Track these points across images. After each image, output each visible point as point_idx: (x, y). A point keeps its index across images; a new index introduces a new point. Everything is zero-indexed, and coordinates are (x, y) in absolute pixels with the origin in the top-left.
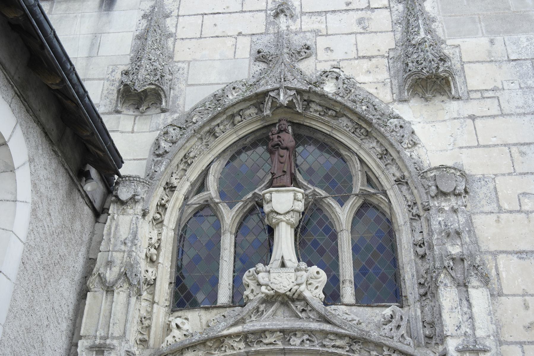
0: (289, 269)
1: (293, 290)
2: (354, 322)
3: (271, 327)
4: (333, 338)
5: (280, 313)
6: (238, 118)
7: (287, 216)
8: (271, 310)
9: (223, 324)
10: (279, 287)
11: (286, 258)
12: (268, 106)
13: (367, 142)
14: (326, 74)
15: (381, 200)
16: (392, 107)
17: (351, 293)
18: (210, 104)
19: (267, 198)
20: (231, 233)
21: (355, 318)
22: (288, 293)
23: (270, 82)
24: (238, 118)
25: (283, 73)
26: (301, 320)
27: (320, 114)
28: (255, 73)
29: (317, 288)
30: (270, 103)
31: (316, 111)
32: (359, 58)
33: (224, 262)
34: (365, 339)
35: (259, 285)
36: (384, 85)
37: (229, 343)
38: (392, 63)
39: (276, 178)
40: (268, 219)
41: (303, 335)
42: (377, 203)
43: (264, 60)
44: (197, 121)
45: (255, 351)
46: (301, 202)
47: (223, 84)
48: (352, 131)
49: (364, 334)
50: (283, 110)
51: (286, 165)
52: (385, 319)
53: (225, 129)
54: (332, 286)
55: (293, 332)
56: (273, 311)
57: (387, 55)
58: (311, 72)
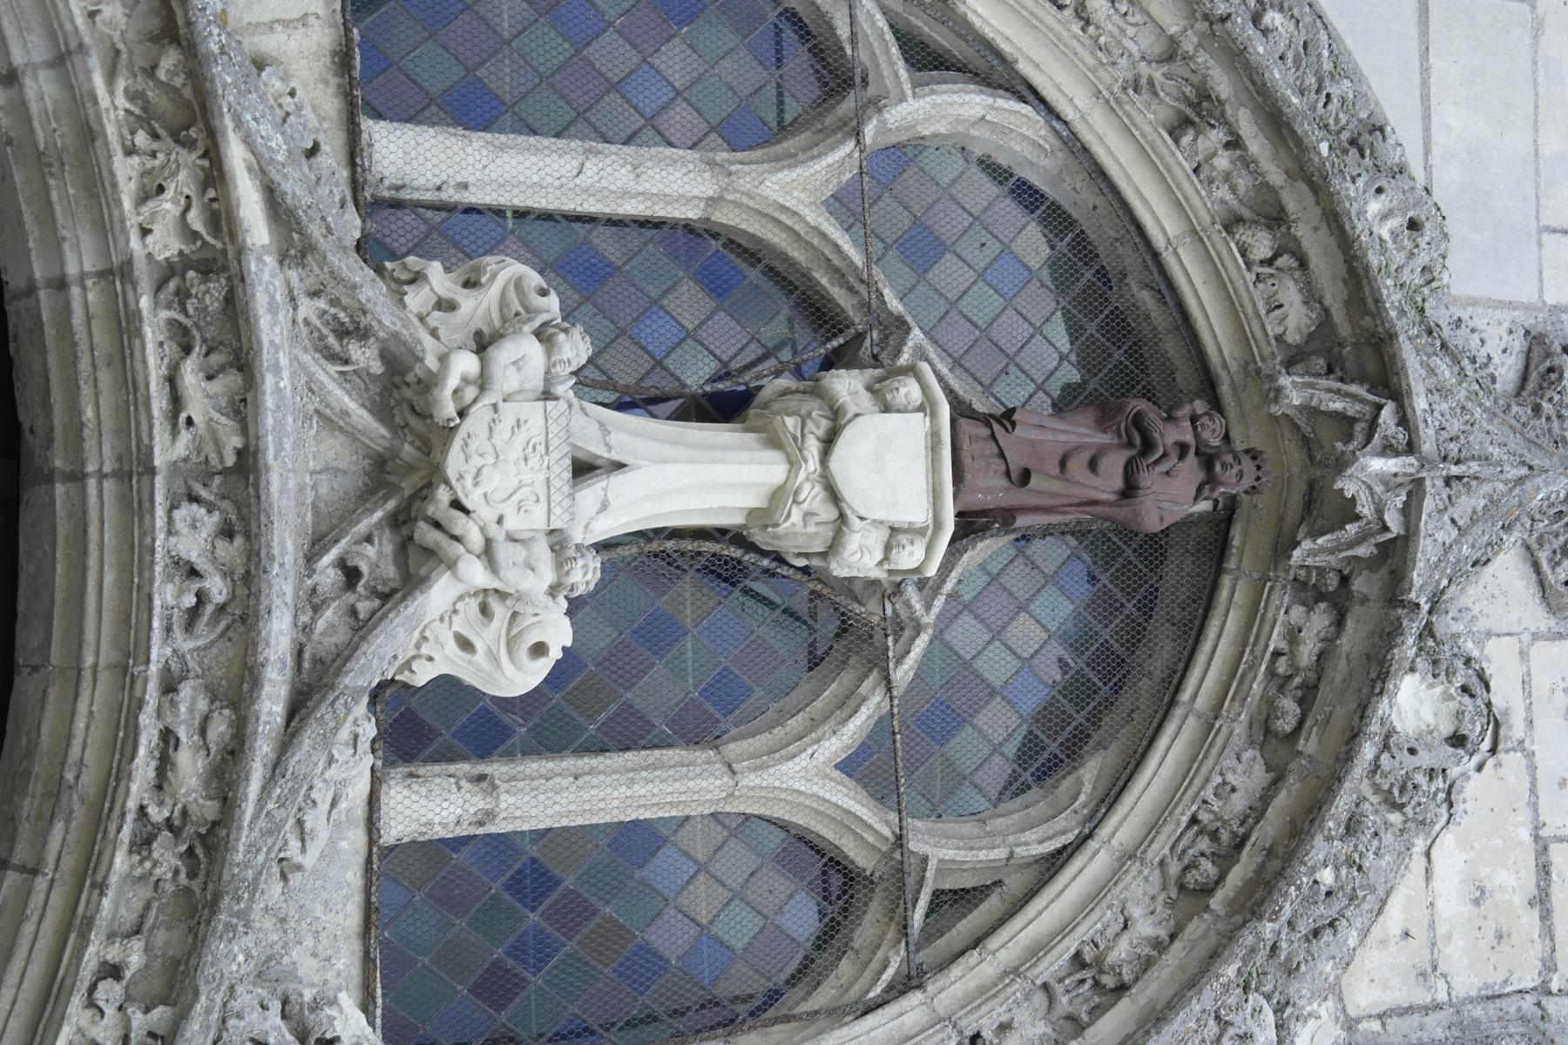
0: (566, 503)
1: (459, 523)
2: (294, 844)
3: (269, 401)
4: (212, 735)
5: (335, 450)
6: (1262, 245)
7: (818, 489)
8: (352, 405)
9: (277, 141)
10: (474, 445)
11: (617, 480)
12: (1323, 395)
13: (1151, 890)
14: (1478, 688)
15: (875, 965)
16: (1323, 1013)
17: (430, 824)
18: (1343, 100)
19: (903, 391)
20: (713, 201)
21: (314, 849)
22: (443, 495)
23: (1444, 407)
24: (1262, 245)
25: (1487, 472)
26: (301, 561)
27: (1277, 654)
28: (1473, 331)
29: (465, 644)
30: (1338, 405)
31: (1293, 635)
32: (1542, 847)
33: (575, 163)
34: (213, 905)
35: (482, 344)
36: (1423, 974)
37: (175, 174)
38: (1519, 1009)
39: (993, 437)
40: (786, 392)
41: (224, 575)
42: (856, 944)
43: (1534, 376)
44: (1265, 32)
45: (134, 316)
46: (880, 563)
47: (1428, 168)
48: (1204, 817)
49: (239, 899)
50: (1295, 470)
51: (1054, 486)
52: (315, 1006)
53: (1211, 181)
54: (458, 723)
55: (245, 520)
56: (345, 413)
57: (1554, 987)
58: (1476, 611)
